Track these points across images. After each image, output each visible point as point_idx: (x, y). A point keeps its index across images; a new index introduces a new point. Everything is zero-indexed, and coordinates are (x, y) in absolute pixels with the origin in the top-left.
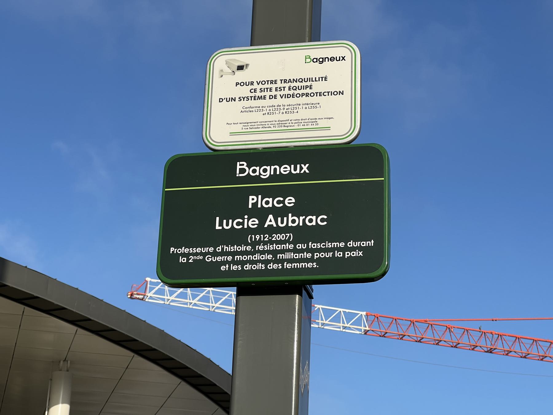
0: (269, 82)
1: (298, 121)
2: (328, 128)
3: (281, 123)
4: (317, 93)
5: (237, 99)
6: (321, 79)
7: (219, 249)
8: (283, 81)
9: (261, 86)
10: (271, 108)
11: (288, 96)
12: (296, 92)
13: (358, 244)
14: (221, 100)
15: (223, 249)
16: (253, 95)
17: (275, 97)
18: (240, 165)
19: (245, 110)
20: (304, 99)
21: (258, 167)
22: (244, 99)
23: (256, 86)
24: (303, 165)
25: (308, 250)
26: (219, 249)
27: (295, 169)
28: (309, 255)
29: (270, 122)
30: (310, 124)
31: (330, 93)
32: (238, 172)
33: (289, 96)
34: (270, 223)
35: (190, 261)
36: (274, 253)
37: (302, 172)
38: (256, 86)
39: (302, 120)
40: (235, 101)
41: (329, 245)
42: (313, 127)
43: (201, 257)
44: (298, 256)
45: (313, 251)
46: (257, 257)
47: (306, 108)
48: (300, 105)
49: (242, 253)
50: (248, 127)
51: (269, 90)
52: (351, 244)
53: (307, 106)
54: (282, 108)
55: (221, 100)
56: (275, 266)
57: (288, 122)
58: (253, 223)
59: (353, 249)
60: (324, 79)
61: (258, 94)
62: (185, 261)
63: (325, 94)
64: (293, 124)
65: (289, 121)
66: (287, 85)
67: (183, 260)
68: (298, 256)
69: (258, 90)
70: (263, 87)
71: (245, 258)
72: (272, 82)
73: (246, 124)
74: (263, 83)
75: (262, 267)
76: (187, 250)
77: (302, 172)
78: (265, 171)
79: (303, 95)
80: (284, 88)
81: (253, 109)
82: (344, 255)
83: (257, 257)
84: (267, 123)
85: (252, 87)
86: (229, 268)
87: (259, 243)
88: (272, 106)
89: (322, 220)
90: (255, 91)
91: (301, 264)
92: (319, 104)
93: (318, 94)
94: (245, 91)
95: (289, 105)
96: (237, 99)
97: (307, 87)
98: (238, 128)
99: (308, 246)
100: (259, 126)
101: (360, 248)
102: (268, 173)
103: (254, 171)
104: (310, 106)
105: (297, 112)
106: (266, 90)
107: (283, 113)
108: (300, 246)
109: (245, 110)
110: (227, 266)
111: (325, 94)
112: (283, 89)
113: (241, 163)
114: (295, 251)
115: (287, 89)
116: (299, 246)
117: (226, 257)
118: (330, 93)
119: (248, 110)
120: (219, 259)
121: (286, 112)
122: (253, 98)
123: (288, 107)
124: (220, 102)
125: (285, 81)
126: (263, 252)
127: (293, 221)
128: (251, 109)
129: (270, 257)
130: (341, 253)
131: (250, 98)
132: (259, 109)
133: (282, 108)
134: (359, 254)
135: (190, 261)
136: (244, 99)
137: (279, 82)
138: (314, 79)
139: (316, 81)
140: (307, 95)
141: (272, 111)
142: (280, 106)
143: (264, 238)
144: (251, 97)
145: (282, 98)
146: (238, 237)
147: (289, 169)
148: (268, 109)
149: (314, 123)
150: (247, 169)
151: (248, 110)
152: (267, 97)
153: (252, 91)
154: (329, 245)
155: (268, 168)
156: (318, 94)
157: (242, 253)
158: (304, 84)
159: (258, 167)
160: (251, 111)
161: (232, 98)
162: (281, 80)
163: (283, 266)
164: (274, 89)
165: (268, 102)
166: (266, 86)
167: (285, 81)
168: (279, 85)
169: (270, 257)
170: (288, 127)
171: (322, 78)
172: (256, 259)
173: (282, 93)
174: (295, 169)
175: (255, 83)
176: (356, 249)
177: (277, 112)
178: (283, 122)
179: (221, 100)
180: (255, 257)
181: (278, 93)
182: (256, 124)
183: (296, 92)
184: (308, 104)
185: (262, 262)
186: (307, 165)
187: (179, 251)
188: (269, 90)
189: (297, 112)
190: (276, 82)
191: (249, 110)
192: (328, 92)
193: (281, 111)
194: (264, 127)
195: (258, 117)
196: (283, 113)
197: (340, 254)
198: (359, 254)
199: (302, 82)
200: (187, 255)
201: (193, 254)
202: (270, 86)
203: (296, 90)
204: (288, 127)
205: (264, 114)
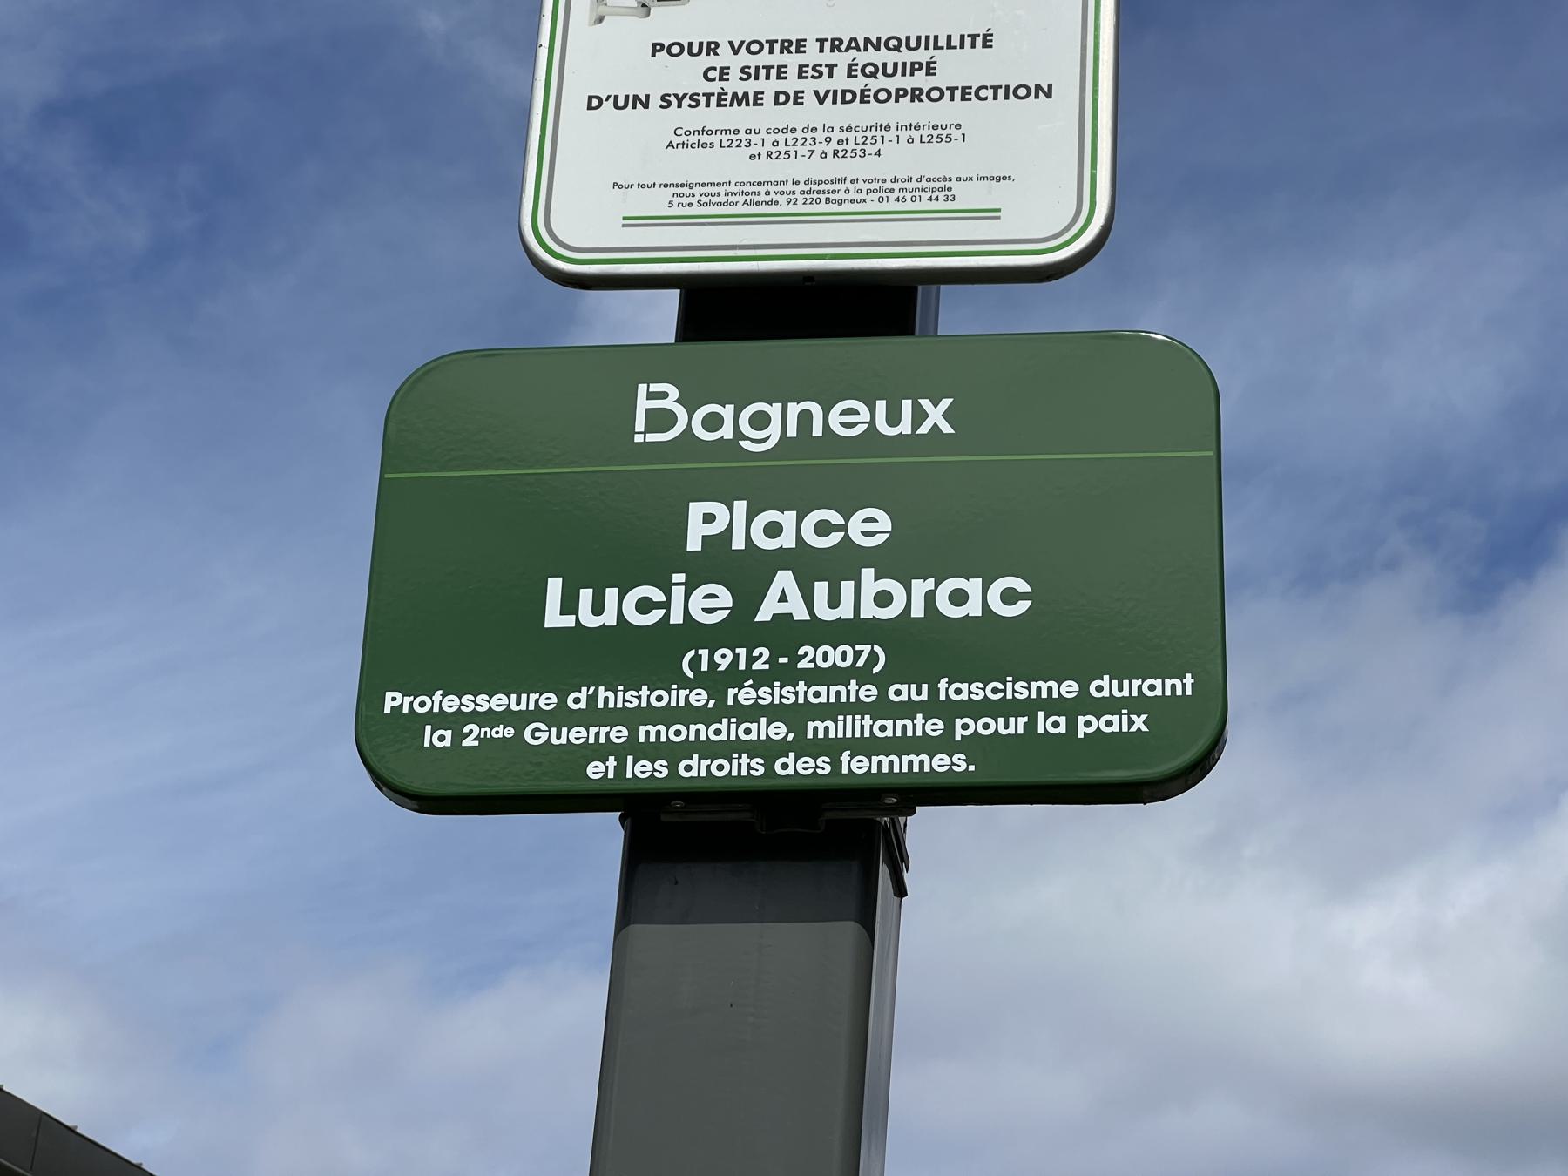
0: (777, 47)
1: (878, 186)
2: (993, 214)
3: (815, 189)
4: (952, 90)
5: (655, 102)
6: (968, 41)
7: (577, 701)
8: (827, 45)
9: (744, 58)
10: (781, 137)
11: (844, 97)
12: (874, 85)
13: (1130, 688)
14: (595, 103)
15: (592, 699)
16: (715, 87)
17: (798, 98)
18: (651, 396)
19: (684, 138)
20: (905, 111)
21: (730, 408)
22: (680, 100)
23: (724, 57)
24: (926, 403)
25: (932, 708)
26: (578, 699)
27: (894, 418)
28: (935, 727)
29: (776, 183)
30: (926, 195)
31: (1001, 92)
32: (640, 425)
33: (849, 97)
34: (783, 609)
35: (467, 742)
36: (796, 715)
37: (924, 429)
38: (724, 57)
39: (894, 180)
40: (646, 106)
41: (1022, 690)
42: (934, 206)
43: (509, 732)
44: (891, 728)
45: (949, 711)
46: (726, 730)
47: (911, 140)
48: (888, 128)
49: (668, 716)
50: (694, 200)
51: (773, 72)
52: (1103, 687)
53: (916, 134)
54: (820, 136)
55: (595, 102)
56: (805, 766)
57: (842, 187)
58: (711, 603)
59: (1111, 705)
60: (979, 41)
61: (735, 85)
62: (447, 743)
63: (983, 93)
64: (863, 196)
65: (848, 185)
66: (842, 59)
67: (430, 737)
68: (891, 728)
69: (735, 74)
70: (753, 61)
71: (678, 733)
72: (785, 47)
73: (686, 190)
74: (755, 47)
75: (749, 768)
76: (450, 703)
77: (924, 429)
78: (760, 421)
79: (900, 94)
80: (831, 67)
81: (715, 139)
82: (1072, 726)
83: (726, 730)
84: (762, 189)
85: (711, 61)
86: (621, 768)
87: (735, 677)
88: (786, 130)
89: (1009, 597)
90: (723, 74)
91: (906, 759)
92: (958, 126)
93: (958, 94)
94: (687, 75)
95: (849, 129)
96: (655, 102)
97: (916, 67)
98: (657, 203)
99: (934, 692)
100: (732, 199)
101: (1136, 704)
102: (774, 431)
103: (713, 422)
104: (925, 133)
105: (878, 153)
106: (763, 72)
107: (824, 155)
108: (901, 692)
109: (684, 138)
110: (612, 762)
111: (983, 93)
112: (825, 71)
113: (655, 387)
114: (882, 709)
115: (841, 71)
116: (898, 693)
117: (604, 730)
118: (1001, 92)
119: (693, 139)
120: (577, 735)
121: (835, 153)
122: (714, 100)
123: (843, 136)
124: (590, 107)
125: (836, 45)
126: (752, 713)
127: (883, 599)
128: (704, 138)
129: (778, 730)
130: (1062, 720)
131: (703, 100)
132: (734, 138)
133: (820, 136)
134: (1131, 723)
135: (467, 742)
136: (680, 100)
137: (812, 47)
138: (942, 42)
139: (949, 46)
140: (916, 95)
141: (782, 148)
142: (814, 130)
143: (751, 660)
144: (708, 96)
145: (821, 101)
146: (649, 654)
147: (865, 414)
148: (770, 138)
149: (941, 195)
150: (680, 411)
151: (693, 139)
152: (768, 99)
153: (711, 74)
154: (1022, 690)
155: (775, 410)
156: (958, 94)
157: (668, 716)
158: (906, 56)
159: (730, 408)
160: (704, 145)
161: (636, 98)
162: (822, 41)
163: (835, 764)
164: (792, 72)
165: (768, 116)
166: (765, 59)
167: (836, 45)
168: (812, 56)
169: (778, 730)
170: (840, 203)
171: (973, 37)
172: (723, 737)
173: (823, 85)
174: (894, 418)
175: (725, 49)
176: (1118, 708)
177: (802, 150)
178: (822, 187)
179: (595, 103)
180: (718, 732)
181: (808, 86)
182: (722, 190)
183: (874, 85)
184: (917, 127)
185: (753, 749)
186: (946, 403)
187: (422, 704)
188: (773, 72)
189: (878, 153)
190: (800, 46)
191: (700, 140)
192: (996, 89)
193: (819, 149)
194: (753, 201)
195: (731, 166)
196: (824, 155)
197: (442, 738)
198: (1131, 723)
199: (897, 48)
200: (456, 721)
201: (474, 717)
202: (777, 59)
203: (873, 75)
204: (840, 203)
205: (752, 157)
